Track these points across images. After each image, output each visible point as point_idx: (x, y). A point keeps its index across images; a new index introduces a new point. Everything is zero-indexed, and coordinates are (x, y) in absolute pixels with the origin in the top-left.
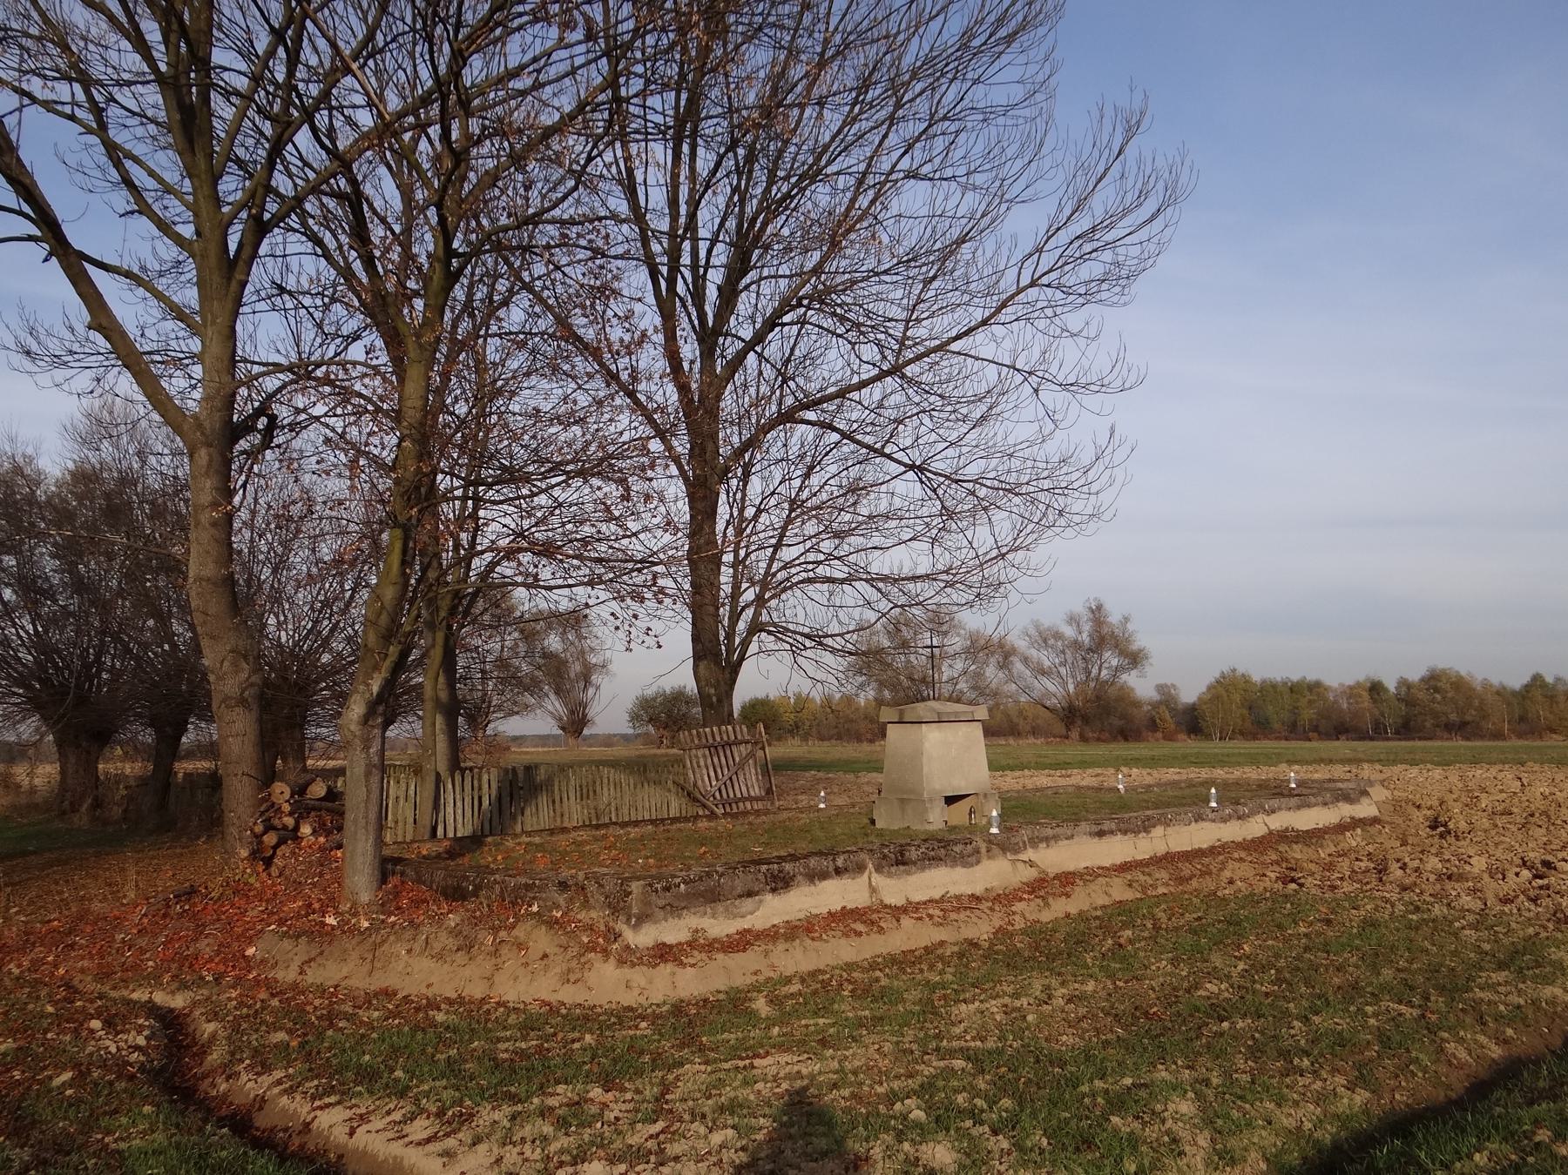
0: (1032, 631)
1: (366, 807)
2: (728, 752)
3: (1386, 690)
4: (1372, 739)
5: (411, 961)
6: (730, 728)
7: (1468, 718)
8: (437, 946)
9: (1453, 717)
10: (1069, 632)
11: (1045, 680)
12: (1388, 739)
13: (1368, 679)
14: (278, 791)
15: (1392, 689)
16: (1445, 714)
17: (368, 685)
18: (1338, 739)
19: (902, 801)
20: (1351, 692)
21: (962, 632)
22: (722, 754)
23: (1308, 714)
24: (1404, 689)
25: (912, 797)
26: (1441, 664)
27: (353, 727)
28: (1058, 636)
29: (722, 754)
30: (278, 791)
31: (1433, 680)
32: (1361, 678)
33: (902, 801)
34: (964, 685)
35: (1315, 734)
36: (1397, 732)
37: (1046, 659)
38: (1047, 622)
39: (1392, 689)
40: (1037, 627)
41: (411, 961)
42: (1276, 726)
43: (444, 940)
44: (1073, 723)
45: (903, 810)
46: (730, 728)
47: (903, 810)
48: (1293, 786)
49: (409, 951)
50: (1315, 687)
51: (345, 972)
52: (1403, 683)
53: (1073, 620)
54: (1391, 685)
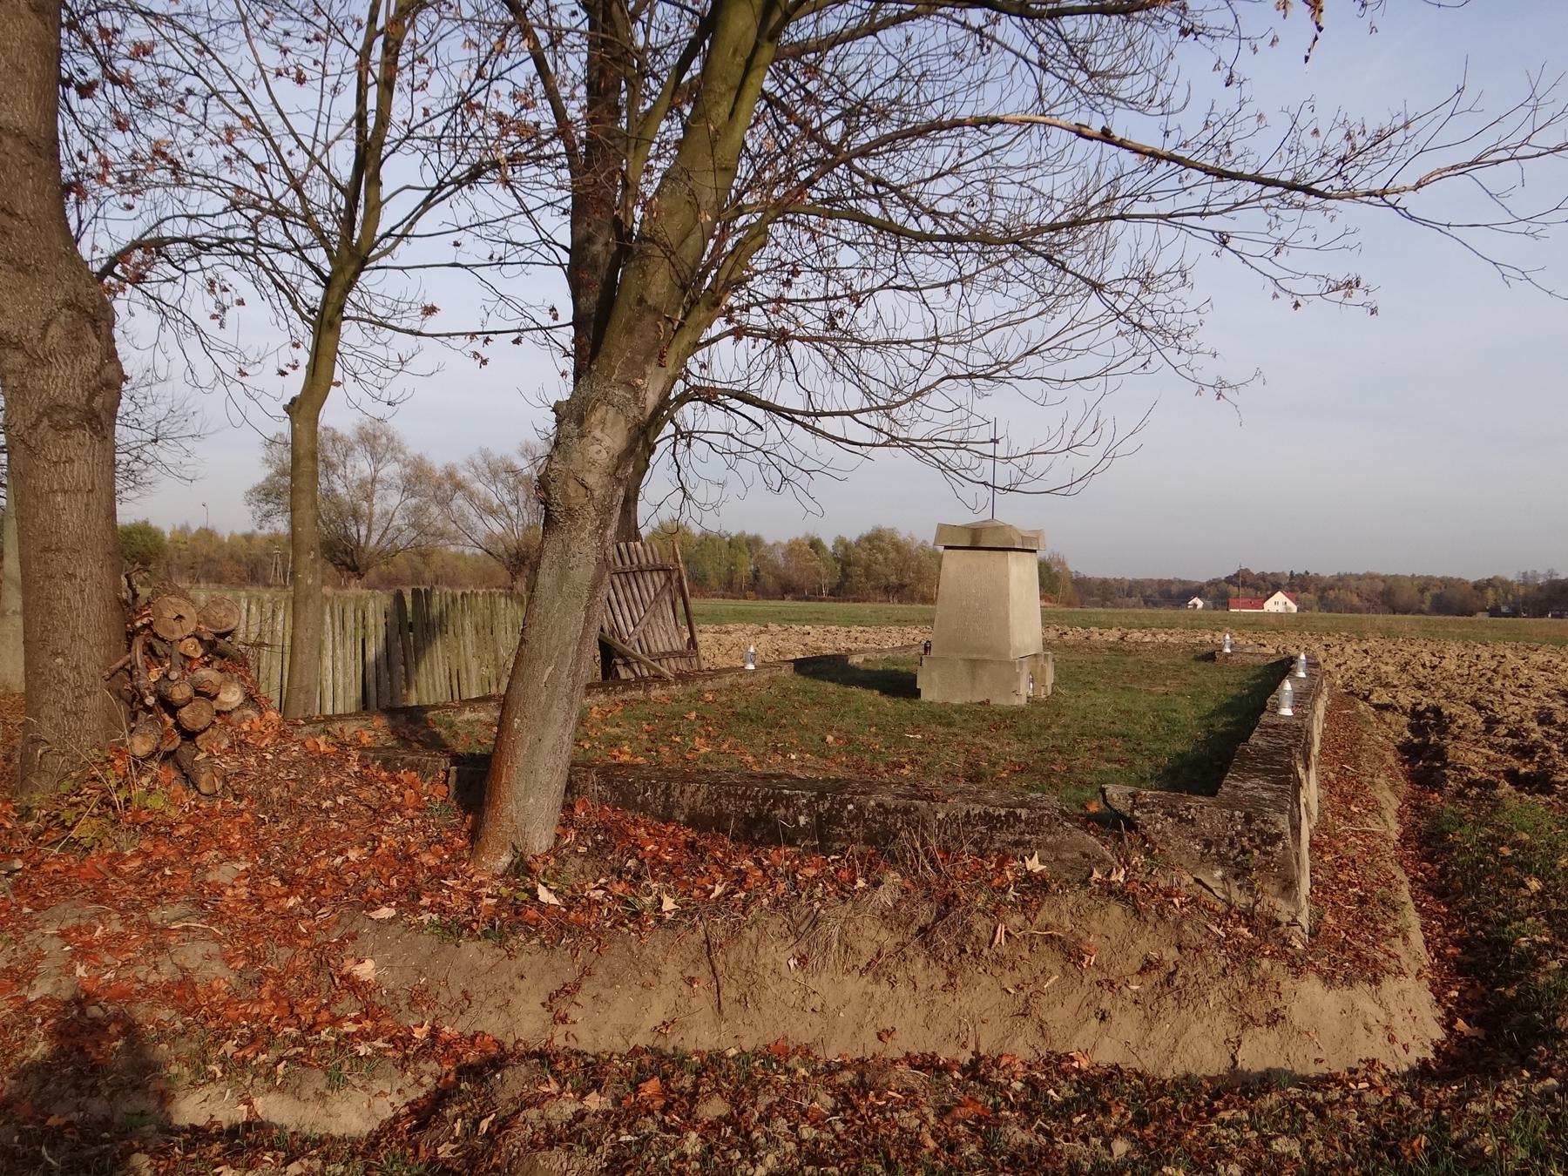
0: (478, 461)
1: (579, 652)
2: (641, 581)
3: (824, 548)
4: (808, 599)
5: (812, 984)
6: (638, 544)
7: (907, 581)
8: (867, 950)
9: (893, 579)
10: (522, 464)
11: (491, 521)
12: (821, 600)
13: (807, 536)
14: (170, 614)
15: (830, 548)
16: (886, 576)
17: (635, 389)
18: (784, 599)
19: (973, 663)
20: (793, 549)
21: (401, 457)
22: (634, 586)
23: (746, 567)
24: (841, 548)
25: (987, 657)
26: (886, 524)
27: (592, 479)
28: (512, 471)
29: (634, 586)
30: (170, 614)
31: (875, 540)
32: (801, 535)
33: (973, 663)
34: (401, 522)
35: (753, 594)
36: (831, 593)
37: (497, 494)
38: (497, 453)
39: (830, 548)
40: (486, 456)
41: (812, 984)
42: (714, 583)
43: (873, 937)
44: (520, 571)
45: (974, 677)
46: (638, 544)
47: (974, 677)
48: (1228, 650)
49: (803, 960)
50: (754, 543)
51: (657, 1013)
52: (841, 542)
53: (526, 451)
54: (829, 543)
